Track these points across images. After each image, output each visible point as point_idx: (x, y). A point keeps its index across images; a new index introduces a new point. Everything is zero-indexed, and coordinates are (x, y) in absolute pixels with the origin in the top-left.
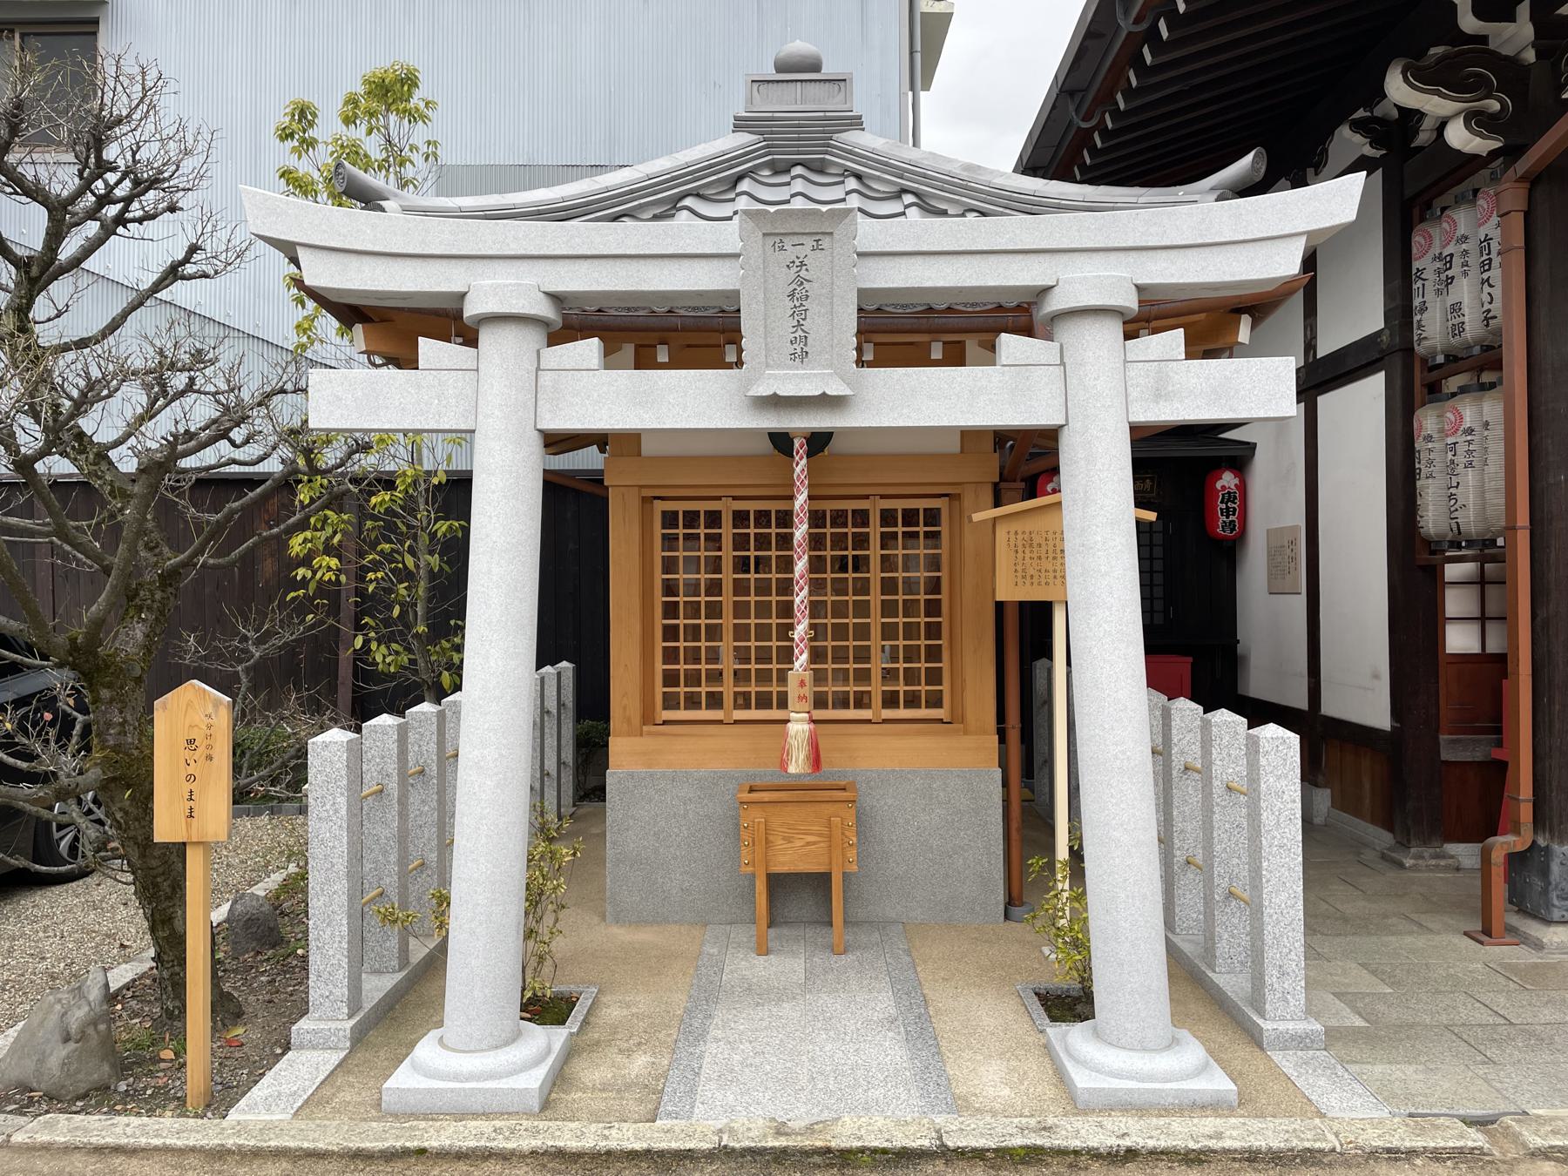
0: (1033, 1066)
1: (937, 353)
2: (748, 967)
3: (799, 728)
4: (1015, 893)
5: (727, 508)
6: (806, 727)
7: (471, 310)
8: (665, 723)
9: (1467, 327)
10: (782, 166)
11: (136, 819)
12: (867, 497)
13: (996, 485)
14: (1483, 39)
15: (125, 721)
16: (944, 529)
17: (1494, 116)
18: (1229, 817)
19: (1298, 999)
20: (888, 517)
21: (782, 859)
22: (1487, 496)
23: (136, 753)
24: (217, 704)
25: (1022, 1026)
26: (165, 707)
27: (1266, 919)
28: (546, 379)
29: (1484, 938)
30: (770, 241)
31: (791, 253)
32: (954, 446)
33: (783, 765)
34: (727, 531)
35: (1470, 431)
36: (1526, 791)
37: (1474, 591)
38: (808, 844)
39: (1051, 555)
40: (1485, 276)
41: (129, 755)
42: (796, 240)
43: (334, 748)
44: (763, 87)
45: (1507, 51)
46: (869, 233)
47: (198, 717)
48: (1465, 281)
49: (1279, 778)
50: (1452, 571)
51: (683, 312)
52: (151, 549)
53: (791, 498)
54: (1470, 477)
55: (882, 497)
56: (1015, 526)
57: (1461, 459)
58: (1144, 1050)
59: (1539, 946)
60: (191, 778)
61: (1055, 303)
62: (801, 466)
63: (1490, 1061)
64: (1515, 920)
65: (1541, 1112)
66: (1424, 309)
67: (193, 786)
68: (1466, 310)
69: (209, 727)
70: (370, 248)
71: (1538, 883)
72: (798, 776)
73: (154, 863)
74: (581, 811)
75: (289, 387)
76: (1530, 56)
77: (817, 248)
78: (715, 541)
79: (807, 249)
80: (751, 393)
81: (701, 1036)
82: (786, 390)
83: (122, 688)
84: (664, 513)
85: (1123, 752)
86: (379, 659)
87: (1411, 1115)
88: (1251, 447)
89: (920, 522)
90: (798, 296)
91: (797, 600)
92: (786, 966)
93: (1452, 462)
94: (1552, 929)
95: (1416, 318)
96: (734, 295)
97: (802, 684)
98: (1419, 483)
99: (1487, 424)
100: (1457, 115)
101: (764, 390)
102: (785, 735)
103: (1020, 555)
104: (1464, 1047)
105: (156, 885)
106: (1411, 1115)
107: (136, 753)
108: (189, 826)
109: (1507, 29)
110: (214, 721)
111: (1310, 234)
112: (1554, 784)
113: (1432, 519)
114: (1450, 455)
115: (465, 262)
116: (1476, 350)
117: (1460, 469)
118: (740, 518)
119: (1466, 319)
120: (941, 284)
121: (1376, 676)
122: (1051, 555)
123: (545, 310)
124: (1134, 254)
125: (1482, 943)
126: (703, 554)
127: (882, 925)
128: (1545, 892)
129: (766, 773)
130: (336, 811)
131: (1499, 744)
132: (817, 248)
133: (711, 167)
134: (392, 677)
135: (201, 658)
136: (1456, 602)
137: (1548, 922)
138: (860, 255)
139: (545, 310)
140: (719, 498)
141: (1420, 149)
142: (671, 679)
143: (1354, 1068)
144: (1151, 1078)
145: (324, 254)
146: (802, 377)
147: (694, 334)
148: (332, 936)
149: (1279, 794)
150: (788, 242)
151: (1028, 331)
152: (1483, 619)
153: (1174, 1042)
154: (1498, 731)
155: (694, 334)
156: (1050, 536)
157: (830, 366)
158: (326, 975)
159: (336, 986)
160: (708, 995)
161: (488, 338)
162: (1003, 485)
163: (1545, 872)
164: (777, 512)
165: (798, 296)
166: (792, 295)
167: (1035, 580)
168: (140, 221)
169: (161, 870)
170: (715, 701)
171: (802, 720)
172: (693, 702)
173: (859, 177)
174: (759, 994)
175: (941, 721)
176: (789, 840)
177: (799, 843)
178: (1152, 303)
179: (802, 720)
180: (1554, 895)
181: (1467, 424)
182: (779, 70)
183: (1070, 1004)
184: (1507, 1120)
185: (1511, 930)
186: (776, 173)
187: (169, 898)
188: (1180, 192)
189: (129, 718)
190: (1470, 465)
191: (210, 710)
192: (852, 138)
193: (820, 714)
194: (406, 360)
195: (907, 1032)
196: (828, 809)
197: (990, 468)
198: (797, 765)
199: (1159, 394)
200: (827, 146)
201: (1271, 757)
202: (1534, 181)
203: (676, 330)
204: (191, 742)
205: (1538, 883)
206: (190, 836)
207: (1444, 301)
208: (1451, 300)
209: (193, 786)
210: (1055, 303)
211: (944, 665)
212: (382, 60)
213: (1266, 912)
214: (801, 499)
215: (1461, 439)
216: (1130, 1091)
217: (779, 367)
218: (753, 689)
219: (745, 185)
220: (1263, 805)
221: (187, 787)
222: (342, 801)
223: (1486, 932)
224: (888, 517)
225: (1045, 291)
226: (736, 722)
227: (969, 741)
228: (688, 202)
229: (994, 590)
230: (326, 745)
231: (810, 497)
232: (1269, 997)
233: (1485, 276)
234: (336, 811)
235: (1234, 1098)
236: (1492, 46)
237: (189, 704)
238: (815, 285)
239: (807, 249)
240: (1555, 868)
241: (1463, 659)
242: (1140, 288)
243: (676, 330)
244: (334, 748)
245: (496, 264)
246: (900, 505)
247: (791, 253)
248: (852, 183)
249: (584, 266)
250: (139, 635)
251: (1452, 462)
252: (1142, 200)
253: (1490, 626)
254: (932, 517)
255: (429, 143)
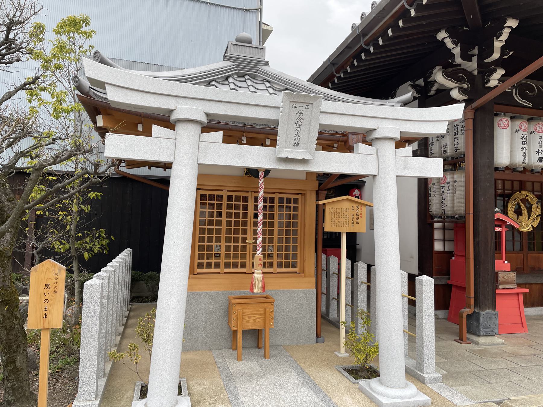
0: (359, 396)
1: (268, 143)
2: (237, 367)
3: (258, 276)
4: (319, 333)
5: (225, 194)
6: (261, 275)
7: (174, 116)
8: (198, 273)
9: (448, 151)
10: (240, 75)
11: (8, 319)
12: (274, 193)
13: (317, 191)
14: (460, 65)
15: (5, 276)
16: (299, 205)
17: (465, 89)
18: (334, 304)
19: (433, 366)
20: (281, 200)
21: (247, 324)
22: (455, 203)
23: (9, 290)
24: (60, 269)
25: (346, 382)
26: (36, 270)
27: (424, 340)
28: (202, 145)
29: (461, 342)
30: (292, 104)
31: (298, 109)
32: (303, 177)
33: (252, 289)
34: (225, 202)
35: (449, 183)
36: (472, 295)
37: (442, 231)
38: (257, 318)
39: (343, 216)
40: (456, 137)
41: (7, 291)
42: (300, 104)
43: (95, 286)
44: (235, 47)
45: (469, 70)
46: (326, 106)
47: (52, 275)
48: (448, 138)
49: (428, 293)
50: (437, 225)
51: (230, 124)
52: (10, 201)
53: (258, 192)
54: (449, 198)
55: (280, 193)
56: (332, 206)
57: (446, 191)
58: (400, 388)
59: (477, 343)
60: (47, 301)
61: (376, 135)
62: (261, 181)
63: (488, 383)
64: (468, 336)
65: (513, 398)
66: (433, 144)
67: (47, 305)
68: (448, 146)
69: (56, 279)
70: (137, 88)
71: (475, 324)
72: (258, 293)
73: (12, 337)
74: (133, 307)
75: (63, 137)
76: (476, 73)
77: (307, 108)
78: (220, 206)
79: (303, 108)
80: (279, 156)
81: (237, 395)
82: (291, 156)
83: (3, 261)
84: (279, 198)
85: (395, 286)
86: (56, 246)
87: (479, 403)
88: (364, 182)
89: (291, 203)
90: (298, 124)
91: (259, 229)
92: (250, 364)
93: (443, 192)
94: (480, 338)
95: (430, 147)
96: (277, 122)
97: (260, 260)
98: (430, 198)
99: (456, 181)
100: (456, 87)
101: (283, 156)
102: (253, 279)
103: (333, 216)
104: (479, 379)
105: (10, 347)
106: (479, 403)
107: (9, 290)
108: (44, 322)
109: (469, 64)
110: (59, 276)
111: (449, 121)
112: (481, 292)
113: (434, 208)
114: (442, 190)
115: (175, 98)
116: (450, 159)
117: (446, 194)
118: (230, 198)
119: (448, 149)
120: (342, 125)
121: (412, 257)
122: (343, 216)
123: (204, 119)
124: (400, 121)
125: (461, 343)
126: (207, 210)
127: (274, 347)
128: (478, 326)
129: (246, 292)
130: (95, 313)
131: (449, 279)
132: (307, 108)
133: (220, 72)
134: (61, 253)
135: (17, 247)
136: (437, 235)
137: (479, 336)
138: (321, 112)
139: (204, 119)
140: (222, 190)
141: (431, 96)
142: (201, 257)
143: (454, 388)
144: (404, 398)
145: (117, 88)
146: (297, 152)
147: (260, 134)
148: (90, 365)
149: (428, 298)
150: (298, 105)
151: (364, 142)
152: (444, 240)
153: (406, 385)
154: (449, 275)
155: (260, 134)
156: (343, 210)
157: (306, 149)
158: (86, 382)
159: (90, 386)
160: (229, 379)
161: (180, 127)
162: (320, 191)
163: (478, 320)
164: (287, 198)
165: (298, 124)
166: (296, 123)
167: (338, 225)
168: (6, 63)
169: (14, 340)
170: (217, 265)
171: (259, 273)
172: (209, 265)
173: (269, 82)
174: (251, 377)
175: (296, 272)
176: (250, 317)
177: (254, 318)
178: (404, 136)
179: (259, 273)
180: (481, 327)
181: (448, 180)
182: (237, 41)
183: (365, 371)
184: (506, 401)
185: (468, 339)
186: (238, 77)
187: (15, 352)
188: (387, 102)
189: (6, 274)
190: (448, 193)
191: (57, 271)
192: (265, 68)
193: (266, 270)
194: (148, 133)
195: (311, 387)
196: (264, 305)
197: (315, 185)
198: (257, 290)
199: (405, 167)
200: (257, 70)
201: (426, 286)
202: (476, 110)
203: (229, 130)
204: (47, 285)
205: (475, 324)
206: (44, 326)
207: (440, 143)
208: (443, 143)
209: (47, 305)
210: (376, 135)
211: (298, 253)
212: (77, 13)
213: (425, 337)
214: (261, 194)
215: (446, 185)
216: (400, 403)
217: (289, 148)
218: (232, 261)
219: (231, 80)
220: (424, 302)
221: (44, 305)
222: (98, 309)
223: (461, 339)
224: (281, 200)
225: (373, 130)
226: (225, 273)
227: (306, 279)
228: (214, 83)
229: (323, 228)
230: (92, 285)
231: (264, 192)
232: (425, 366)
233: (456, 137)
234: (95, 313)
235: (430, 402)
236: (462, 67)
237: (48, 269)
238: (305, 121)
239: (303, 108)
240: (481, 319)
241: (439, 252)
242: (401, 132)
243: (229, 130)
244: (95, 286)
245: (187, 100)
246: (285, 196)
247: (298, 109)
248: (268, 85)
249: (253, 108)
250: (8, 238)
251: (443, 192)
252: (374, 103)
253: (446, 243)
254: (296, 201)
255: (90, 46)
